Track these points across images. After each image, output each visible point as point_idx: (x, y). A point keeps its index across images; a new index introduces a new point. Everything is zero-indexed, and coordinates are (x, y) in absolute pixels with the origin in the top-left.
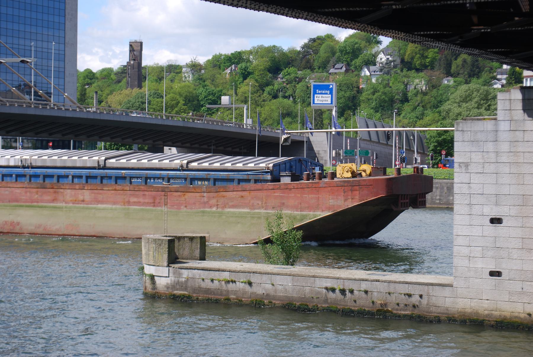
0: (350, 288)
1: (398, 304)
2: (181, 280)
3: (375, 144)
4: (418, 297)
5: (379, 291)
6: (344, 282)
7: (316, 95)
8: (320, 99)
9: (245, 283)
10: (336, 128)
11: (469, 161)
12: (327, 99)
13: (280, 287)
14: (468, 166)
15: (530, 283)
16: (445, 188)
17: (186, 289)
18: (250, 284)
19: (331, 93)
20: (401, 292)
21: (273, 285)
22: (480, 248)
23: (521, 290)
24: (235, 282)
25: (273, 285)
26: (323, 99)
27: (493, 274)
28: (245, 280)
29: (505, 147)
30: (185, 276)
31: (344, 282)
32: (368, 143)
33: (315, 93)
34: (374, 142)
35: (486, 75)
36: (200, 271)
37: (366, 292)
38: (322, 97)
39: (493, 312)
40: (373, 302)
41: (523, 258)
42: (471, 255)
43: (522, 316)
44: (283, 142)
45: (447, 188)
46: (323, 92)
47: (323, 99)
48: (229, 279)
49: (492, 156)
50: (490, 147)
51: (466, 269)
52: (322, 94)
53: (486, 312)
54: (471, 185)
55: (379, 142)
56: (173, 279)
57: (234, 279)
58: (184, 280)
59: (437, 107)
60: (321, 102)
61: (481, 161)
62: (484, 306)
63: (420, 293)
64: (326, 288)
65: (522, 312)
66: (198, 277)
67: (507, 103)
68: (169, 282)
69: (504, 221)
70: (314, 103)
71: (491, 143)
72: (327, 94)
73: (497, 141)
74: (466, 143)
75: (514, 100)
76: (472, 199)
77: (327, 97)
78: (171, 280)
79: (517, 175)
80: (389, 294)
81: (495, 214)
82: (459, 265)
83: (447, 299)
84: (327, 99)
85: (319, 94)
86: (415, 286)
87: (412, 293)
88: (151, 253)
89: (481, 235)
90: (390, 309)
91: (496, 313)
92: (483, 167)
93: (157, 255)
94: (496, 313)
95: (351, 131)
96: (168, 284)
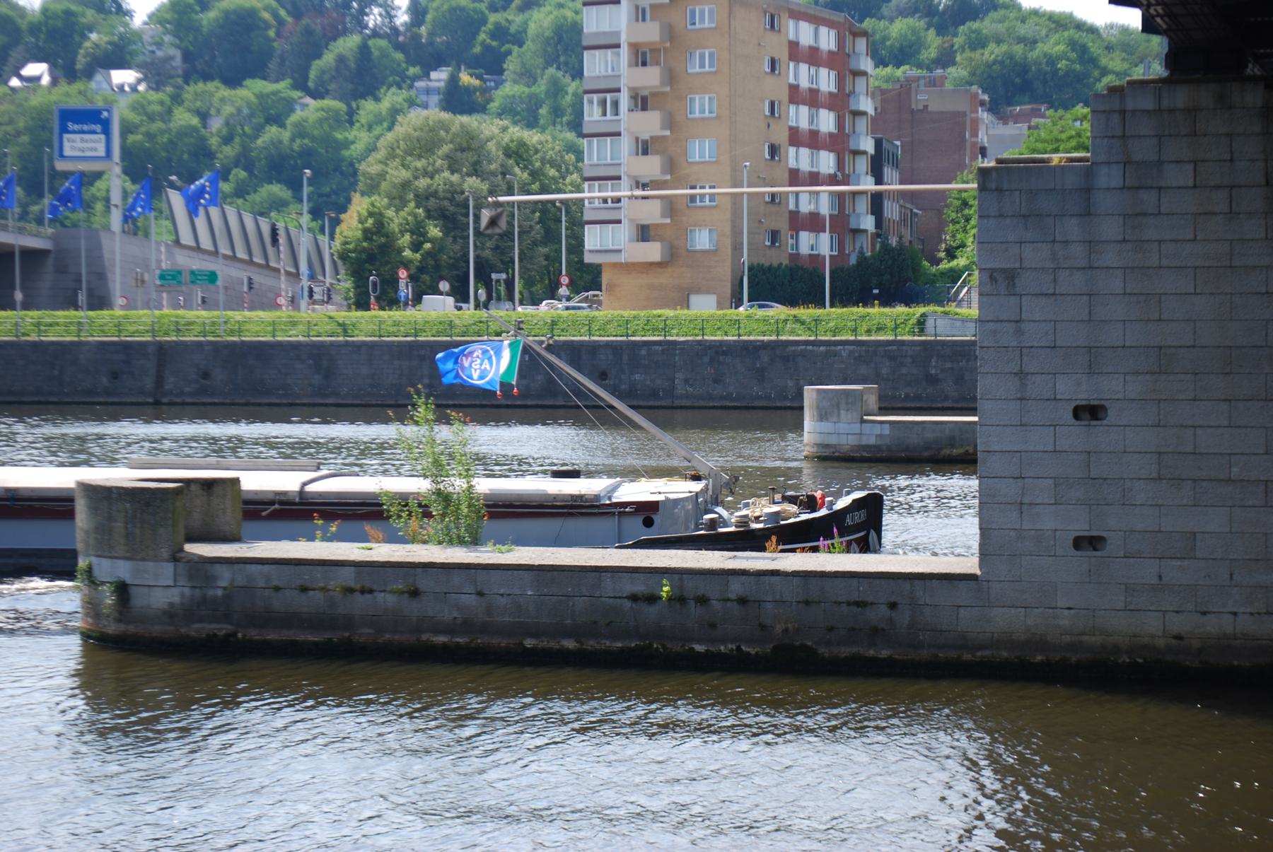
2: (211, 593)
4: (884, 610)
5: (778, 597)
6: (681, 580)
7: (66, 136)
8: (80, 145)
9: (403, 593)
10: (879, 181)
11: (1018, 265)
12: (93, 145)
13: (503, 601)
14: (1013, 278)
17: (227, 618)
18: (415, 593)
19: (106, 131)
20: (840, 599)
21: (480, 594)
22: (1051, 481)
23: (1155, 581)
24: (371, 591)
25: (480, 594)
27: (1079, 543)
29: (1110, 228)
30: (224, 583)
31: (681, 580)
33: (64, 130)
34: (225, 257)
37: (742, 601)
38: (82, 140)
39: (1085, 638)
41: (1160, 502)
42: (1026, 500)
46: (85, 127)
48: (352, 584)
50: (1072, 228)
51: (1012, 534)
53: (1067, 639)
54: (1023, 325)
55: (251, 262)
56: (187, 591)
57: (368, 585)
58: (220, 592)
61: (1048, 264)
63: (892, 600)
64: (634, 598)
68: (177, 600)
69: (1111, 412)
71: (1074, 221)
72: (94, 132)
74: (1008, 221)
75: (1134, 111)
76: (1025, 359)
78: (182, 595)
79: (1142, 298)
80: (807, 603)
81: (1084, 395)
83: (962, 611)
84: (93, 145)
85: (74, 132)
86: (877, 581)
87: (870, 599)
88: (119, 525)
91: (1093, 639)
92: (1055, 280)
93: (138, 531)
94: (1093, 639)
96: (171, 605)
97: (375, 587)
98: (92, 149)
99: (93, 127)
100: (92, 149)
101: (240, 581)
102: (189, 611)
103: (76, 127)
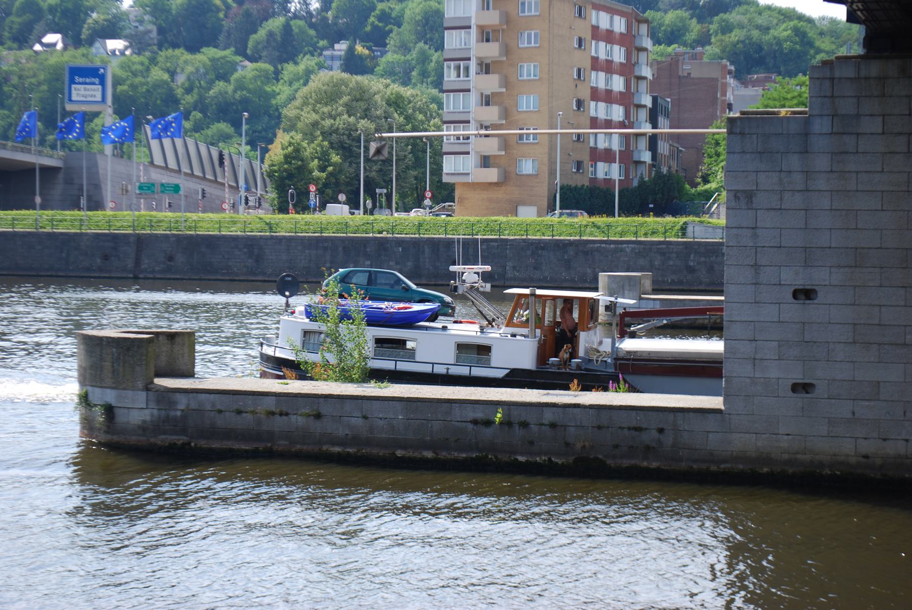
0: (522, 420)
1: (616, 446)
2: (172, 413)
3: (173, 174)
4: (654, 434)
5: (578, 423)
6: (509, 409)
7: (73, 86)
8: (83, 92)
11: (754, 188)
12: (93, 93)
13: (381, 423)
15: (867, 403)
16: (341, 249)
17: (184, 431)
18: (318, 416)
19: (103, 83)
20: (623, 425)
21: (365, 417)
22: (776, 343)
23: (850, 416)
24: (287, 414)
25: (365, 417)
26: (87, 93)
27: (795, 388)
28: (307, 411)
29: (822, 162)
31: (509, 409)
32: (162, 171)
33: (72, 82)
35: (305, 59)
36: (217, 396)
37: (553, 425)
38: (85, 89)
39: (799, 456)
40: (567, 444)
41: (854, 359)
42: (758, 357)
43: (853, 460)
44: (374, 155)
45: (344, 248)
46: (88, 80)
47: (87, 93)
48: (274, 410)
49: (798, 178)
50: (794, 162)
51: (748, 380)
52: (86, 83)
54: (757, 231)
56: (155, 412)
57: (285, 410)
58: (179, 413)
59: (314, 111)
60: (84, 99)
62: (782, 445)
63: (660, 426)
64: (475, 422)
65: (853, 454)
66: (209, 407)
67: (827, 83)
68: (148, 418)
70: (70, 100)
71: (796, 156)
72: (94, 84)
73: (807, 152)
74: (748, 156)
75: (840, 78)
77: (94, 90)
78: (152, 415)
79: (844, 213)
81: (801, 282)
82: (735, 375)
83: (711, 435)
84: (93, 93)
85: (80, 83)
86: (650, 413)
88: (107, 364)
89: (776, 319)
90: (600, 457)
91: (805, 457)
92: (781, 199)
95: (557, 134)
96: (144, 422)
97: (290, 411)
98: (92, 96)
99: (93, 80)
100: (92, 96)
101: (193, 405)
102: (156, 427)
103: (81, 80)
